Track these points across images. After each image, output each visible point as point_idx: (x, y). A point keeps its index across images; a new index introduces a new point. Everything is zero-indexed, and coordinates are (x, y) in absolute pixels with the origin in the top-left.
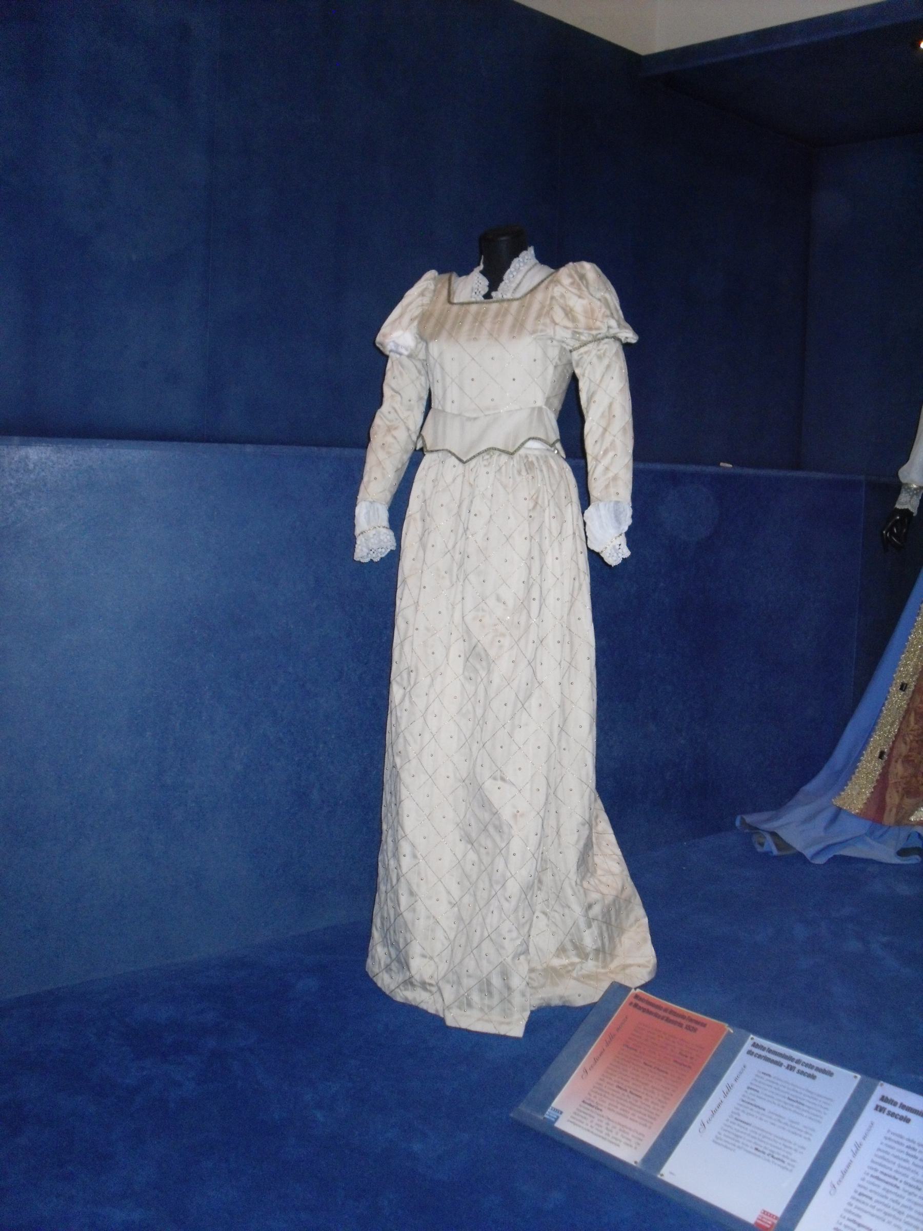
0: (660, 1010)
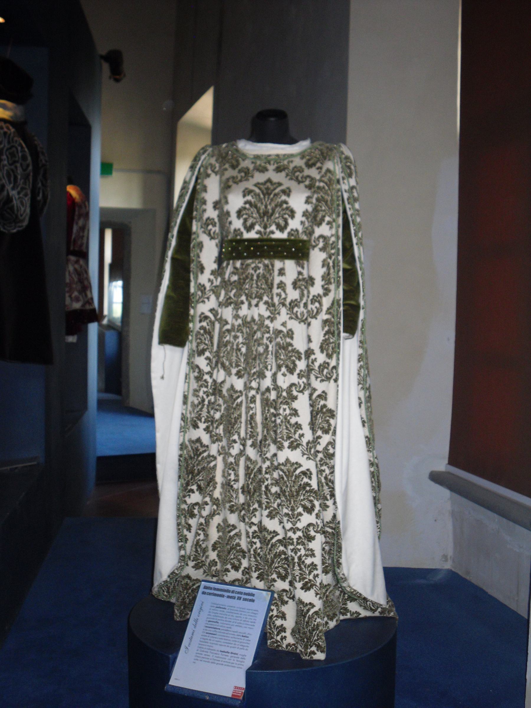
0: (241, 594)
